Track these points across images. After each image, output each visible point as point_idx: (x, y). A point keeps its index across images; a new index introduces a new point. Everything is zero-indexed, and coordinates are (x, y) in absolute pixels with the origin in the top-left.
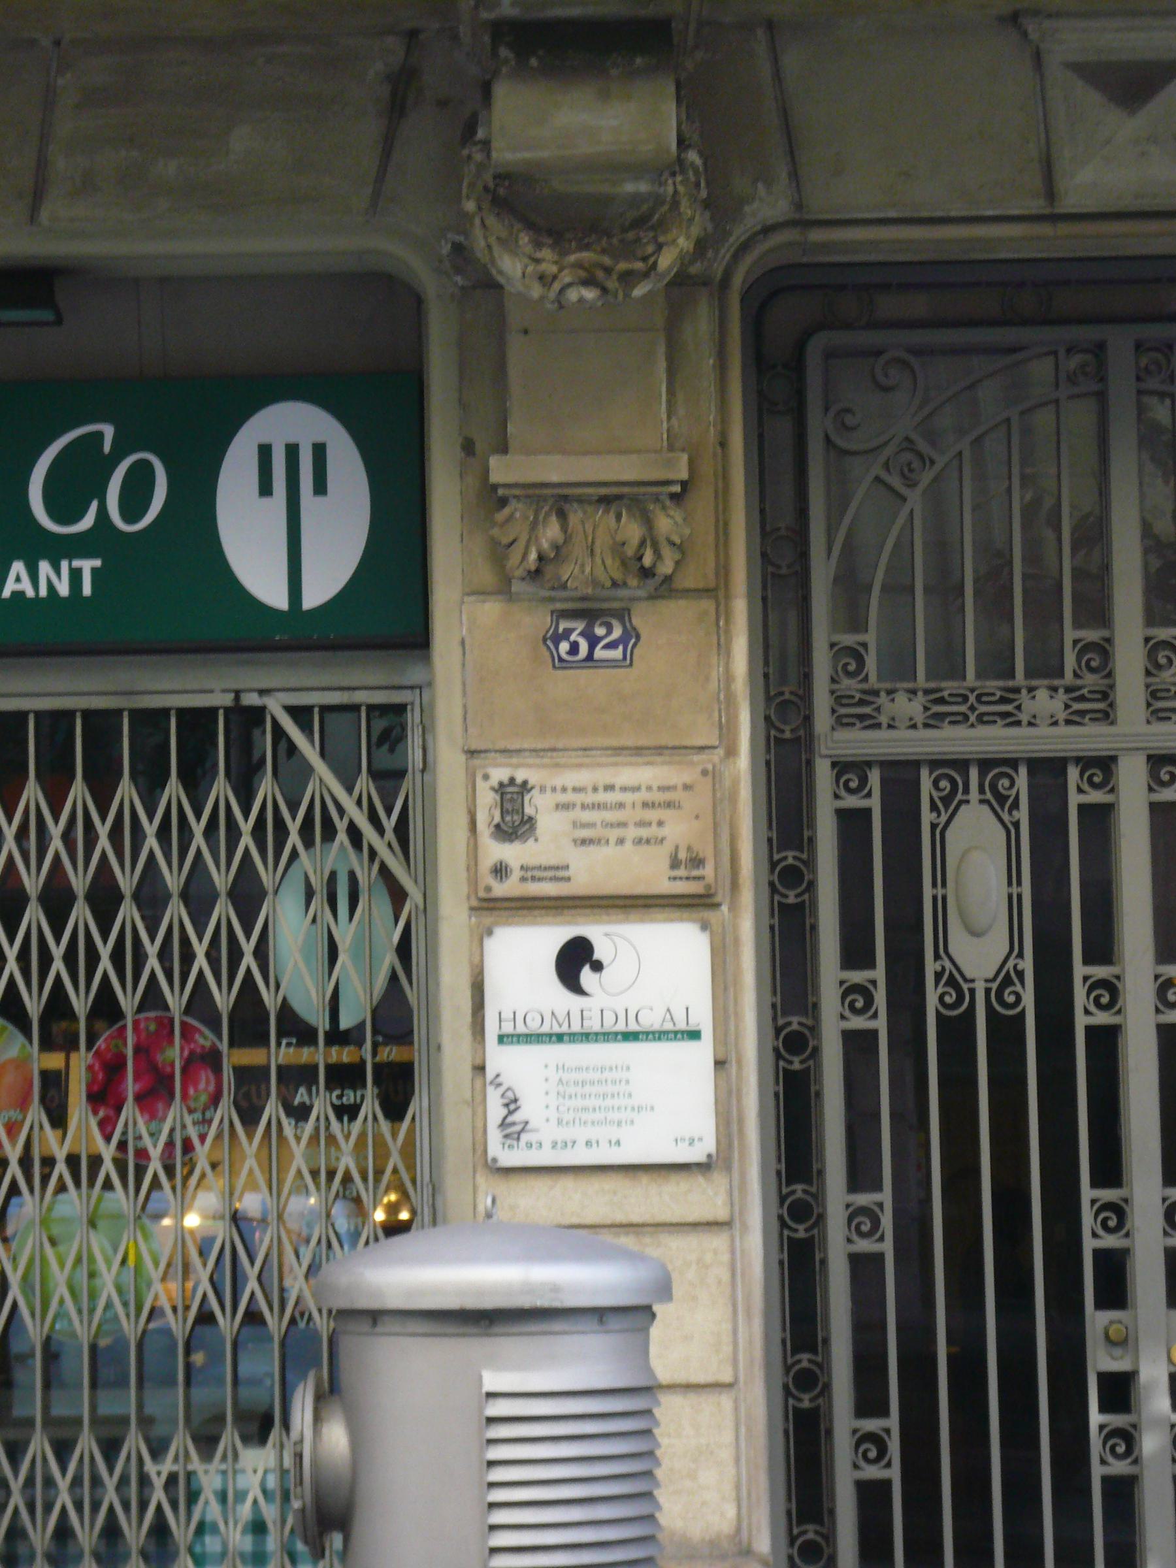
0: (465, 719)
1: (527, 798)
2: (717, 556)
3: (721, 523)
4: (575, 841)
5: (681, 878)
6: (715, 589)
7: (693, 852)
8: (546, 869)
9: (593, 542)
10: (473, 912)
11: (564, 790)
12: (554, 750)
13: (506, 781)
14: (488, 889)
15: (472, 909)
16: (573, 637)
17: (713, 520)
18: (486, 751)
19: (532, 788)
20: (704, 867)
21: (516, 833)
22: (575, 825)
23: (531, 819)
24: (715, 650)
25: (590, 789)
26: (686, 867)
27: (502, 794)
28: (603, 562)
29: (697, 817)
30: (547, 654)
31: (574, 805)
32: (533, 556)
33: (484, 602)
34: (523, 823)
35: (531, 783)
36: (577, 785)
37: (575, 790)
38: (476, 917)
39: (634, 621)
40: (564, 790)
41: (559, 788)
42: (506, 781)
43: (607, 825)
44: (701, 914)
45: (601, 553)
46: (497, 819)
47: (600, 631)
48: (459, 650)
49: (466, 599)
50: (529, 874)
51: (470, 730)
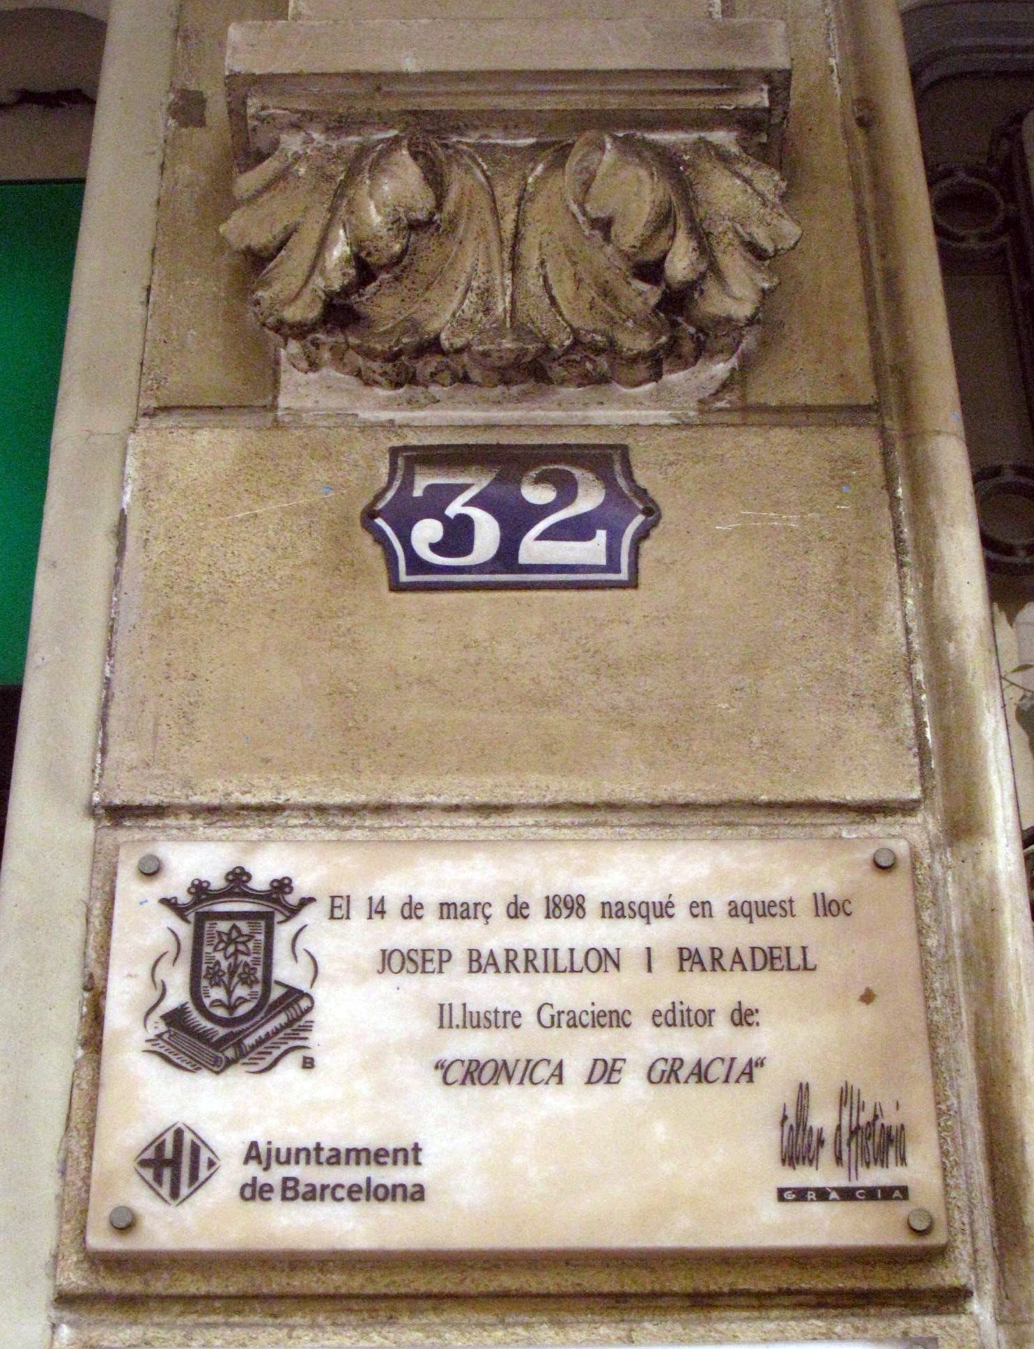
0: (104, 719)
1: (283, 933)
2: (875, 342)
3: (878, 276)
4: (443, 1067)
5: (822, 1195)
6: (876, 408)
7: (861, 1107)
8: (336, 1158)
9: (517, 236)
10: (68, 1315)
11: (412, 910)
12: (384, 809)
13: (217, 881)
14: (126, 1224)
15: (65, 1300)
16: (454, 509)
17: (855, 257)
18: (159, 811)
19: (306, 902)
20: (903, 1160)
21: (234, 1040)
22: (444, 1017)
23: (293, 995)
24: (888, 548)
25: (498, 911)
26: (839, 1159)
27: (202, 919)
28: (547, 286)
29: (868, 997)
30: (374, 553)
31: (445, 957)
32: (339, 250)
33: (193, 430)
34: (265, 1008)
35: (303, 885)
36: (458, 896)
37: (448, 910)
38: (71, 1324)
39: (641, 477)
40: (412, 910)
41: (393, 906)
42: (217, 881)
43: (555, 1022)
44: (901, 1324)
45: (542, 263)
46: (178, 995)
47: (537, 494)
48: (104, 548)
49: (141, 420)
50: (276, 1175)
51: (114, 752)
